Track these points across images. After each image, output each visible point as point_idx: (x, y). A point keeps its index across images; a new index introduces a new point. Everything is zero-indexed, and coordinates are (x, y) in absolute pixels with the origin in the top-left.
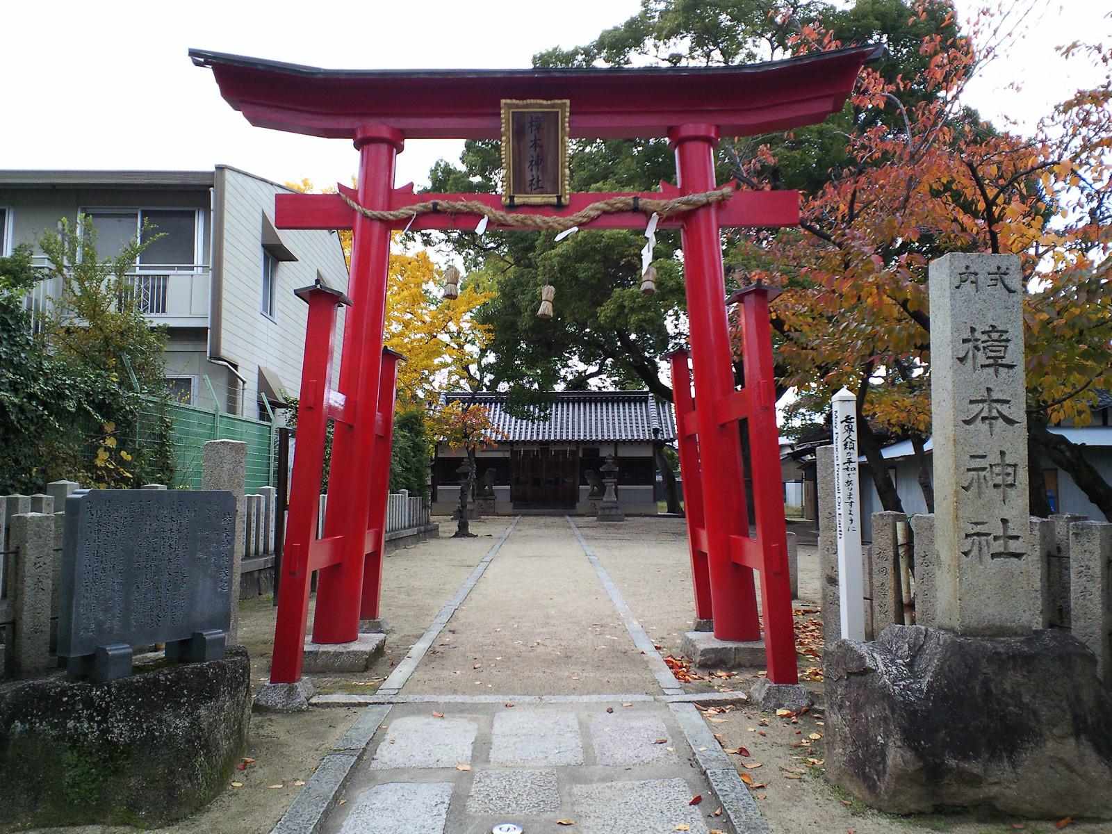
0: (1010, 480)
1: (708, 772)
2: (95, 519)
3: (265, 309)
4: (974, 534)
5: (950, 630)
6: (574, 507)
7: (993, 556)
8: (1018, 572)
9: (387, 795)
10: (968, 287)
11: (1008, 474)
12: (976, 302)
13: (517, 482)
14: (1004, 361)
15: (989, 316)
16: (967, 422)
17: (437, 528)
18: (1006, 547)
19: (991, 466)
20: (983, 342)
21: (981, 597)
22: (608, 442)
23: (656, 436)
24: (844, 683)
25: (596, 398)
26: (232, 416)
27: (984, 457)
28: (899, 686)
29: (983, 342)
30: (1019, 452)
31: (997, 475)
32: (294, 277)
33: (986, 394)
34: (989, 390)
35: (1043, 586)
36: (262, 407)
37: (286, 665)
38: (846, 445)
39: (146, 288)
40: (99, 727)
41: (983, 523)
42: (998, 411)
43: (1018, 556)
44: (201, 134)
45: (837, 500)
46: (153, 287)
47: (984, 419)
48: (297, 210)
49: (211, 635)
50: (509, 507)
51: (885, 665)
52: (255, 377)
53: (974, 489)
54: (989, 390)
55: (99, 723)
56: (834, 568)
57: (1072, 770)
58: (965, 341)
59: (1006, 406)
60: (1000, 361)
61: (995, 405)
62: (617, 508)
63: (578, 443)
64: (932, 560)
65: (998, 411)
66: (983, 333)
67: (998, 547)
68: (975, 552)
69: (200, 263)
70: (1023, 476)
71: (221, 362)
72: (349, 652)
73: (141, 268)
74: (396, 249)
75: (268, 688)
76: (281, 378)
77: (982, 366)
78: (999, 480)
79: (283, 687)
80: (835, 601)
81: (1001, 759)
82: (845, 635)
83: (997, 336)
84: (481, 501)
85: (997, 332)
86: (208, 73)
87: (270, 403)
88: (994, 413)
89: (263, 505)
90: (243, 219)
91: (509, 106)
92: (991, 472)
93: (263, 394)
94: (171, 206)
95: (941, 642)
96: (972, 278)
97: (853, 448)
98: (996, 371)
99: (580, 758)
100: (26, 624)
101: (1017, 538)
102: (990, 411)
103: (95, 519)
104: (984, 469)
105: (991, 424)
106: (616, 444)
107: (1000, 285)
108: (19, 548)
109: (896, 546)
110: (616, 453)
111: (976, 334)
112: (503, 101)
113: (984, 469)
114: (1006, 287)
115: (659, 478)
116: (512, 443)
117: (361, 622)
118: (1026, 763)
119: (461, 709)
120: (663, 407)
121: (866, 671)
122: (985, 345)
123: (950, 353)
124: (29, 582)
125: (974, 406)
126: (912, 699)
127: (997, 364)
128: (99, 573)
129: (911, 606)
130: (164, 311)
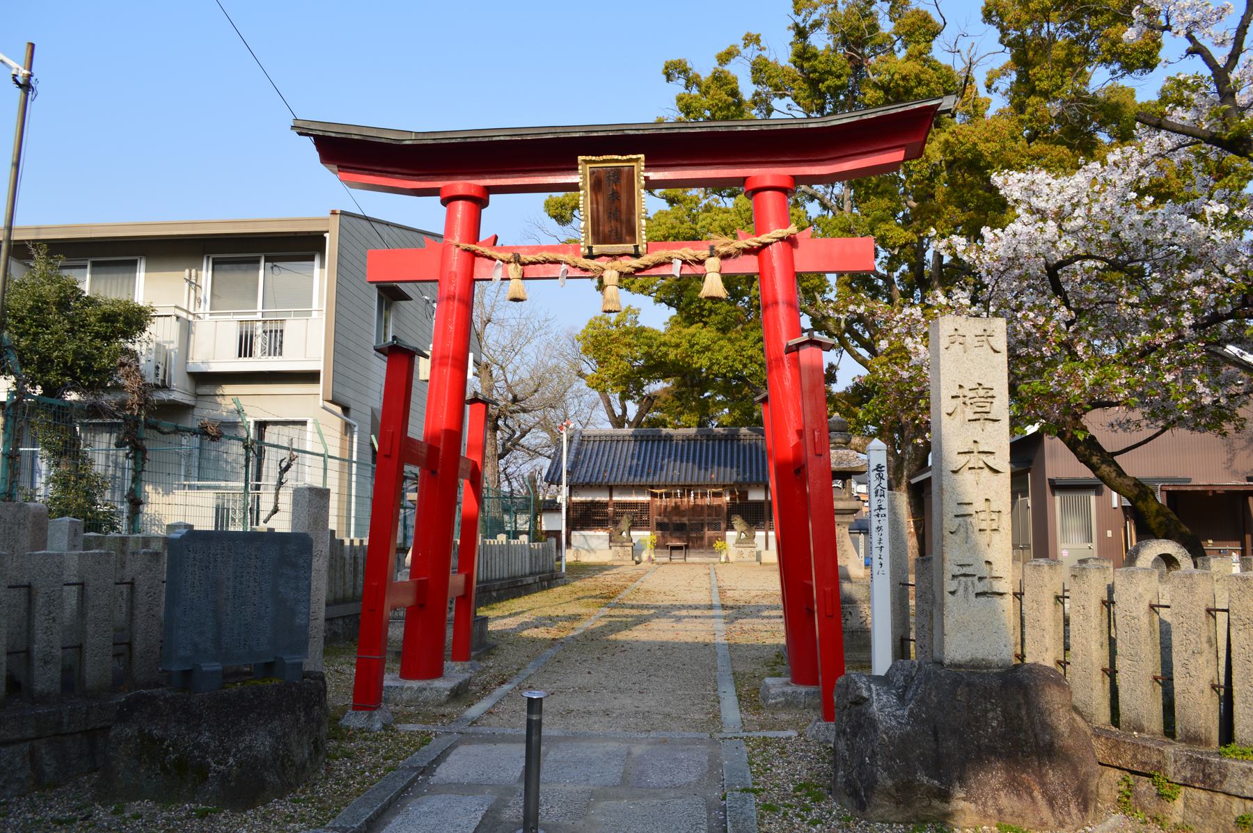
7: (978, 595)
9: (435, 802)
14: (990, 416)
49: (289, 659)
59: (991, 457)
68: (961, 592)
86: (309, 143)
91: (586, 162)
96: (961, 340)
107: (986, 346)
112: (580, 158)
119: (209, 488)
130: (281, 354)
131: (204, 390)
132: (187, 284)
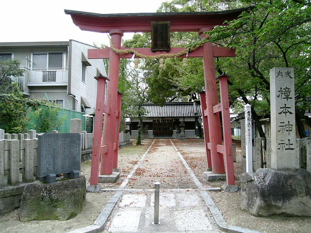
0: (291, 129)
1: (210, 208)
2: (45, 141)
3: (82, 80)
4: (281, 144)
5: (275, 169)
6: (171, 136)
7: (286, 149)
8: (292, 153)
10: (280, 77)
11: (290, 127)
12: (282, 81)
13: (155, 129)
14: (289, 97)
15: (286, 84)
16: (280, 113)
17: (132, 143)
18: (289, 147)
19: (286, 125)
20: (284, 92)
21: (283, 161)
22: (182, 117)
23: (196, 115)
24: (246, 184)
25: (175, 104)
26: (74, 111)
27: (284, 123)
28: (260, 184)
29: (284, 92)
30: (293, 121)
31: (287, 127)
32: (91, 72)
33: (284, 106)
34: (285, 105)
35: (299, 157)
36: (82, 108)
37: (94, 180)
38: (248, 119)
39: (50, 75)
40: (49, 195)
41: (283, 141)
42: (288, 111)
43: (293, 149)
44: (67, 31)
45: (246, 135)
46: (52, 74)
47: (284, 112)
48: (95, 53)
50: (153, 136)
51: (257, 179)
52: (80, 100)
53: (281, 131)
54: (285, 105)
55: (49, 194)
56: (245, 153)
57: (305, 205)
58: (279, 91)
60: (288, 97)
61: (287, 109)
62: (184, 136)
63: (172, 117)
64: (270, 151)
65: (288, 111)
66: (284, 89)
67: (287, 147)
69: (65, 67)
70: (294, 128)
71: (71, 96)
72: (110, 177)
73: (49, 69)
74: (237, 151)
75: (90, 186)
76: (87, 100)
77: (283, 98)
78: (287, 129)
79: (93, 186)
80: (245, 163)
81: (286, 202)
82: (247, 171)
83: (288, 90)
84: (144, 135)
85: (288, 89)
86: (69, 16)
87: (85, 107)
88: (287, 111)
89: (83, 136)
90: (76, 54)
92: (286, 127)
93: (83, 104)
94: (57, 51)
95: (272, 173)
96: (281, 74)
97: (250, 120)
98: (287, 100)
99: (175, 205)
100: (27, 169)
101: (292, 144)
102: (286, 110)
103: (45, 141)
104: (284, 126)
105: (286, 114)
106: (184, 117)
107: (288, 76)
108: (25, 148)
109: (262, 147)
110: (184, 120)
111: (282, 89)
113: (284, 126)
114: (290, 77)
115: (197, 127)
116: (153, 118)
117: (113, 169)
118: (293, 203)
120: (198, 106)
121: (252, 181)
122: (284, 92)
123: (275, 95)
124: (28, 157)
125: (281, 109)
126: (264, 187)
127: (287, 98)
128: (47, 155)
129: (266, 163)
130: (55, 81)
131: (32, 91)
132: (27, 61)
